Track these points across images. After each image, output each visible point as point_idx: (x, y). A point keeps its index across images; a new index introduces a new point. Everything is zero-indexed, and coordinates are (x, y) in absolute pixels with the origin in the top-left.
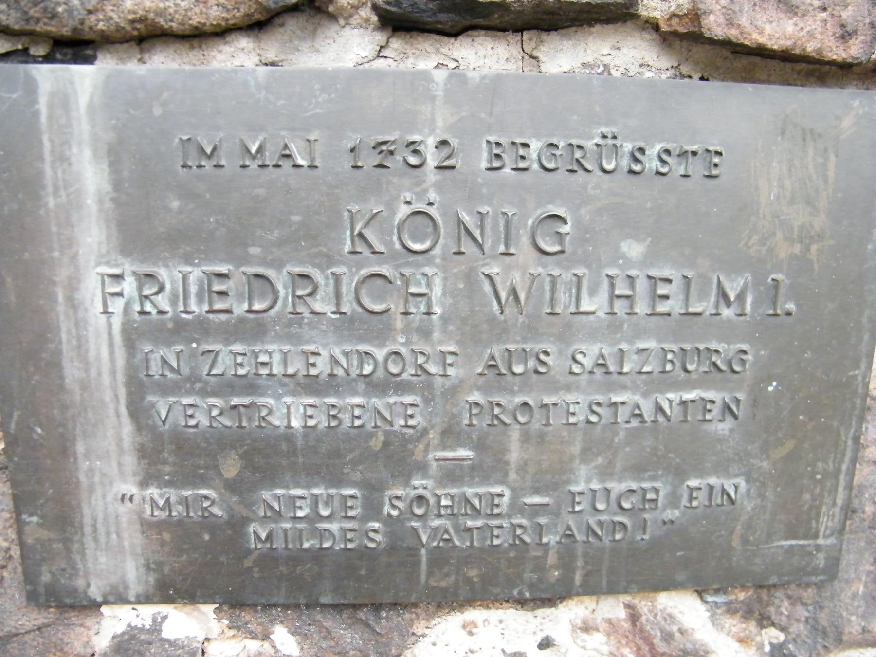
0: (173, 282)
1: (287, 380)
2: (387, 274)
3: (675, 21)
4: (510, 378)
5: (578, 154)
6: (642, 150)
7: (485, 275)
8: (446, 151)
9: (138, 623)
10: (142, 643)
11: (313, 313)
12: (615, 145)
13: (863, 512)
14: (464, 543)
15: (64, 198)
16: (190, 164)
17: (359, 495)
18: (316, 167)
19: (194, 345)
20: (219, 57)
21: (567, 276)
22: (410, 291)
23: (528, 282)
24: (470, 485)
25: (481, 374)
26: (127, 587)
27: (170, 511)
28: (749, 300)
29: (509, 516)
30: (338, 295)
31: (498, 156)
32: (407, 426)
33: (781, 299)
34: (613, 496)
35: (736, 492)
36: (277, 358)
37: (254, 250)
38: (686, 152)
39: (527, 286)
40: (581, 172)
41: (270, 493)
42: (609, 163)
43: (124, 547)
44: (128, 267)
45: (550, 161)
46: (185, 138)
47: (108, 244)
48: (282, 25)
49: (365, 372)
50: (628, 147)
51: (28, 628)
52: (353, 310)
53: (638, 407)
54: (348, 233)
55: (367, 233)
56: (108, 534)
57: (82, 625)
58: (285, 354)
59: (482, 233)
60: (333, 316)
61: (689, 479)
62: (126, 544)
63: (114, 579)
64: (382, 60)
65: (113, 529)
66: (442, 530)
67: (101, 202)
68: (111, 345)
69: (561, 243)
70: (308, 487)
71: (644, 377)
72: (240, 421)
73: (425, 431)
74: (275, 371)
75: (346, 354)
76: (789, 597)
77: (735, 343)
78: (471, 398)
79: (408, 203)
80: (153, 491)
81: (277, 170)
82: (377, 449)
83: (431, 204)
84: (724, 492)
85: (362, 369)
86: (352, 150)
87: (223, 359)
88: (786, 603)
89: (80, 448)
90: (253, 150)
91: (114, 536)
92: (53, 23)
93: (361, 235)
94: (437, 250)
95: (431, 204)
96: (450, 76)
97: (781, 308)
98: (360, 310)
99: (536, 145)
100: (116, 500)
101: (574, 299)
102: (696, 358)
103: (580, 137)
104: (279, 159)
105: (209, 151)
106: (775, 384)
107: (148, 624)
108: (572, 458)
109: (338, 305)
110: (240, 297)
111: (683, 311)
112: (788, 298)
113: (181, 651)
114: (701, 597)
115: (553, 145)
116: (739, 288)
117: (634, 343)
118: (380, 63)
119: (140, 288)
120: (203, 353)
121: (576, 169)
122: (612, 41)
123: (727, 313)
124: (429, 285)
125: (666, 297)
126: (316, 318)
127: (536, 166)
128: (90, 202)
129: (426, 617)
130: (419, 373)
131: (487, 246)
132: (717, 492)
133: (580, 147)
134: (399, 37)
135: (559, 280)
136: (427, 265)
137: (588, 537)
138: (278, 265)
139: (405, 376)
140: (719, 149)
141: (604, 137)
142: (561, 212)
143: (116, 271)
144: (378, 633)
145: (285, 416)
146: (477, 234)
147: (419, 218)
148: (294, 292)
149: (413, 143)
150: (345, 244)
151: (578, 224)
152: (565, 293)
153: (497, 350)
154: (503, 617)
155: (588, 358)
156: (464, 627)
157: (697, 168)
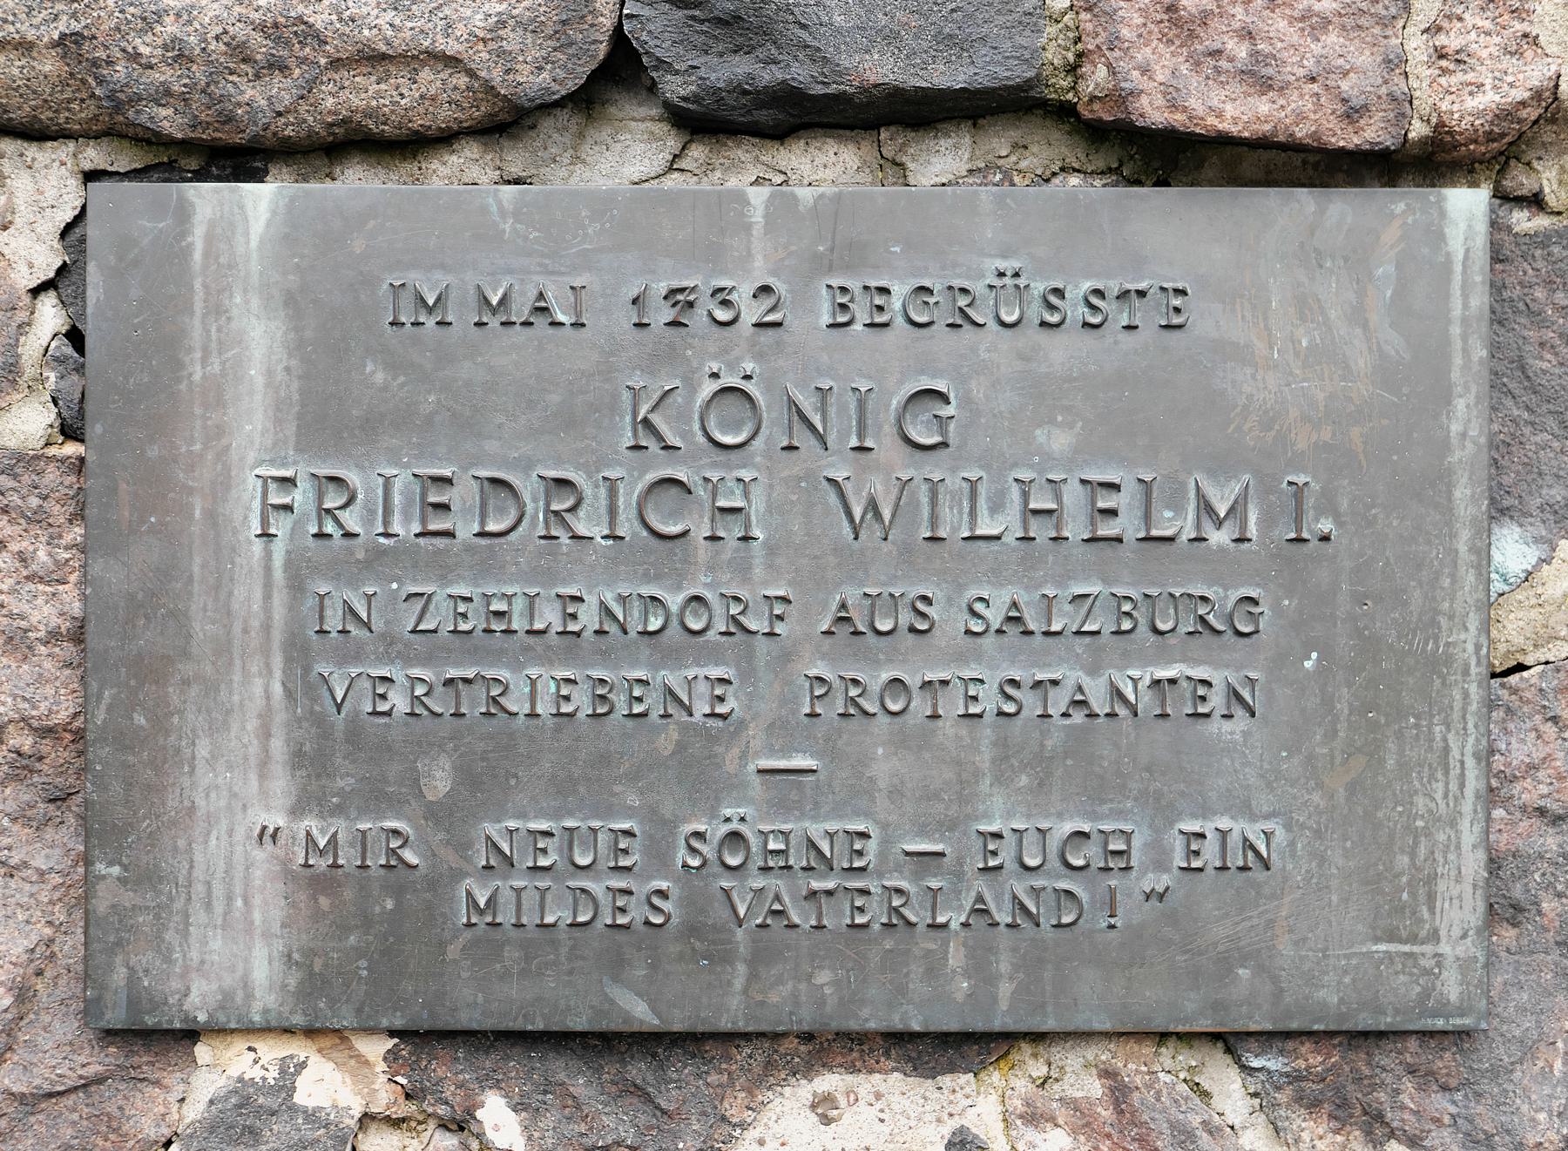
0: (369, 490)
1: (531, 640)
2: (685, 479)
3: (1096, 106)
4: (871, 638)
5: (962, 302)
6: (1059, 292)
7: (829, 480)
8: (768, 302)
9: (256, 1073)
10: (259, 1112)
11: (575, 537)
12: (1017, 287)
13: (1539, 913)
14: (807, 920)
15: (217, 368)
16: (403, 319)
17: (636, 830)
18: (583, 325)
19: (395, 586)
20: (443, 171)
21: (954, 482)
22: (719, 504)
23: (895, 492)
24: (815, 819)
25: (828, 633)
26: (249, 996)
27: (336, 856)
28: (1253, 518)
29: (881, 875)
30: (612, 511)
31: (843, 307)
32: (713, 715)
33: (1309, 515)
34: (1053, 844)
35: (1268, 845)
36: (519, 605)
37: (492, 446)
38: (1128, 291)
39: (893, 497)
40: (967, 327)
41: (497, 826)
42: (1010, 313)
43: (252, 923)
44: (298, 469)
45: (920, 314)
46: (397, 283)
47: (276, 433)
48: (533, 127)
49: (651, 628)
50: (1039, 287)
51: (70, 1083)
52: (634, 535)
53: (1080, 689)
54: (628, 419)
55: (656, 419)
56: (230, 899)
57: (157, 1083)
58: (531, 599)
59: (824, 421)
60: (603, 542)
61: (1182, 820)
62: (257, 916)
63: (228, 981)
64: (676, 175)
65: (238, 890)
66: (771, 896)
67: (270, 373)
68: (268, 585)
69: (943, 430)
70: (557, 815)
71: (1088, 639)
72: (458, 705)
73: (742, 724)
74: (515, 626)
75: (622, 600)
76: (1412, 1071)
77: (1236, 588)
78: (813, 672)
79: (715, 376)
80: (311, 823)
81: (528, 330)
82: (666, 753)
83: (748, 377)
84: (1248, 845)
85: (645, 624)
86: (635, 301)
87: (437, 608)
88: (1408, 1085)
89: (203, 750)
90: (495, 301)
91: (239, 903)
92: (227, 128)
93: (645, 421)
94: (758, 443)
95: (748, 377)
96: (772, 196)
97: (1310, 531)
98: (645, 533)
99: (900, 290)
100: (249, 837)
101: (966, 517)
102: (1172, 611)
103: (968, 278)
104: (531, 313)
105: (431, 302)
106: (1314, 655)
107: (273, 1074)
108: (977, 774)
109: (612, 523)
110: (466, 511)
111: (1142, 535)
112: (1320, 512)
113: (322, 1131)
114: (1238, 1061)
115: (923, 289)
116: (1233, 498)
117: (1067, 587)
118: (673, 181)
119: (320, 499)
120: (410, 596)
121: (959, 322)
122: (1014, 134)
123: (1219, 538)
124: (746, 494)
125: (1113, 513)
126: (578, 545)
127: (900, 321)
128: (255, 373)
129: (746, 1084)
130: (733, 630)
131: (831, 439)
132: (1234, 840)
133: (964, 291)
134: (701, 141)
135: (941, 489)
136: (744, 466)
137: (1014, 917)
138: (526, 465)
139: (711, 635)
140: (1180, 286)
141: (1001, 275)
142: (941, 386)
143: (288, 473)
144: (664, 1112)
145: (527, 698)
146: (817, 420)
147: (730, 399)
148: (548, 504)
149: (722, 290)
150: (622, 436)
151: (966, 401)
152: (951, 508)
153: (852, 594)
154: (882, 1088)
155: (992, 609)
156: (813, 1107)
157: (1149, 316)
